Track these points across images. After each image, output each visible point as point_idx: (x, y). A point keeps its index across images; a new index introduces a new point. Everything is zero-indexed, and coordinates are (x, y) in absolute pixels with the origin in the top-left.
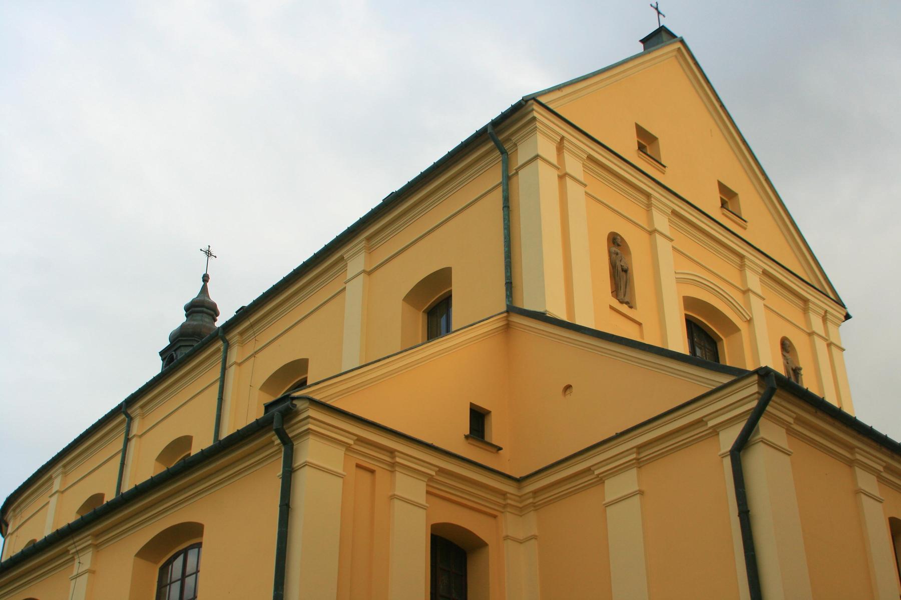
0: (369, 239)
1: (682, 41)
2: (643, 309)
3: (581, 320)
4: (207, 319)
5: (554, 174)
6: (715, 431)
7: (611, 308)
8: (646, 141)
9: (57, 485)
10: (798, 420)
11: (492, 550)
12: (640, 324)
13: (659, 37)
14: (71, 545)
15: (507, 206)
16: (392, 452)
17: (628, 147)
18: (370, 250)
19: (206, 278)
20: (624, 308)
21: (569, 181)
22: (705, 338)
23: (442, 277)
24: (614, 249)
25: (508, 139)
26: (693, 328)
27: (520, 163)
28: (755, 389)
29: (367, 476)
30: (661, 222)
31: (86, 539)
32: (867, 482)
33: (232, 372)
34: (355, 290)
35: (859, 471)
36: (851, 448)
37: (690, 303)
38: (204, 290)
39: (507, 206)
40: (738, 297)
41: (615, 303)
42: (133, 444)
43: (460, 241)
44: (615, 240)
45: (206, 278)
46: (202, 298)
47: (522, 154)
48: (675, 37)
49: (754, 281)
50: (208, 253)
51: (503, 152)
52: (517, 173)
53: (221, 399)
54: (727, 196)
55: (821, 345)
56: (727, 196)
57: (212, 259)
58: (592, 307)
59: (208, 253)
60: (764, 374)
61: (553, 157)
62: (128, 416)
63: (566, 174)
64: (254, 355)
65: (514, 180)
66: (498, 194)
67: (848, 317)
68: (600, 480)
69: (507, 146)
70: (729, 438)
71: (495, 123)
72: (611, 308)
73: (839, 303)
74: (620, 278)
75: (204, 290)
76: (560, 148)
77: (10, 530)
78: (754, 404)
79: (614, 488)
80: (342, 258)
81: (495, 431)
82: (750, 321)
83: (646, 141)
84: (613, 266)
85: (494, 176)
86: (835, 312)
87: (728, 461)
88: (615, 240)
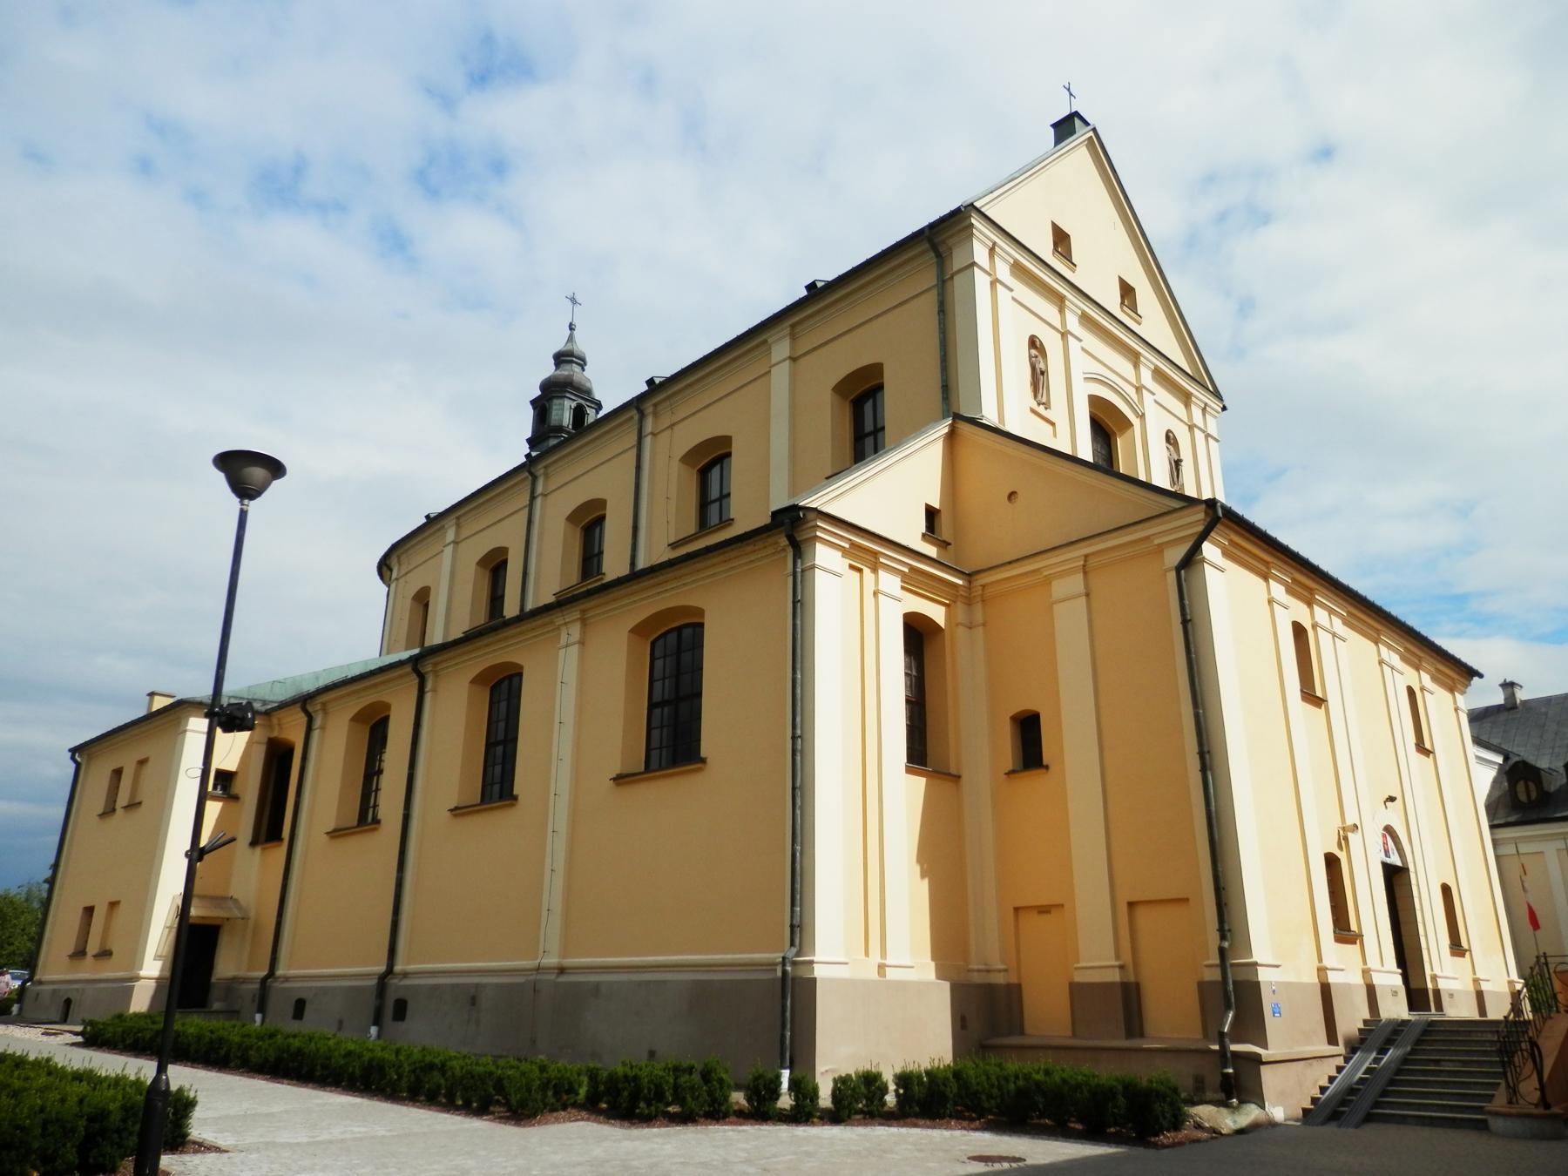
0: (793, 326)
1: (1094, 130)
2: (1058, 412)
3: (1010, 427)
4: (577, 369)
6: (1160, 548)
7: (1033, 411)
8: (1061, 239)
9: (450, 535)
12: (1053, 424)
13: (1065, 128)
16: (876, 554)
17: (1043, 245)
19: (571, 327)
20: (1041, 410)
21: (999, 286)
23: (875, 370)
24: (1034, 352)
27: (955, 268)
28: (1201, 516)
29: (857, 575)
30: (1073, 323)
31: (574, 614)
32: (1278, 590)
34: (780, 377)
37: (1095, 401)
38: (571, 339)
39: (943, 309)
40: (1132, 392)
42: (539, 501)
43: (890, 338)
44: (1034, 342)
45: (571, 327)
46: (569, 347)
47: (957, 262)
48: (1087, 124)
49: (1147, 377)
50: (573, 301)
51: (939, 255)
52: (952, 277)
53: (638, 468)
54: (1127, 291)
55: (1199, 435)
56: (1127, 291)
57: (577, 308)
59: (573, 301)
60: (1211, 504)
62: (531, 474)
63: (997, 280)
64: (671, 426)
65: (949, 284)
66: (932, 298)
67: (1224, 408)
69: (942, 249)
70: (1175, 555)
71: (932, 226)
72: (1033, 411)
73: (1217, 394)
74: (1038, 378)
75: (571, 339)
76: (992, 251)
77: (394, 575)
78: (1200, 528)
79: (1060, 588)
80: (765, 342)
82: (1142, 416)
83: (1061, 239)
84: (1033, 368)
85: (930, 278)
86: (1215, 404)
87: (1172, 576)
88: (1034, 342)
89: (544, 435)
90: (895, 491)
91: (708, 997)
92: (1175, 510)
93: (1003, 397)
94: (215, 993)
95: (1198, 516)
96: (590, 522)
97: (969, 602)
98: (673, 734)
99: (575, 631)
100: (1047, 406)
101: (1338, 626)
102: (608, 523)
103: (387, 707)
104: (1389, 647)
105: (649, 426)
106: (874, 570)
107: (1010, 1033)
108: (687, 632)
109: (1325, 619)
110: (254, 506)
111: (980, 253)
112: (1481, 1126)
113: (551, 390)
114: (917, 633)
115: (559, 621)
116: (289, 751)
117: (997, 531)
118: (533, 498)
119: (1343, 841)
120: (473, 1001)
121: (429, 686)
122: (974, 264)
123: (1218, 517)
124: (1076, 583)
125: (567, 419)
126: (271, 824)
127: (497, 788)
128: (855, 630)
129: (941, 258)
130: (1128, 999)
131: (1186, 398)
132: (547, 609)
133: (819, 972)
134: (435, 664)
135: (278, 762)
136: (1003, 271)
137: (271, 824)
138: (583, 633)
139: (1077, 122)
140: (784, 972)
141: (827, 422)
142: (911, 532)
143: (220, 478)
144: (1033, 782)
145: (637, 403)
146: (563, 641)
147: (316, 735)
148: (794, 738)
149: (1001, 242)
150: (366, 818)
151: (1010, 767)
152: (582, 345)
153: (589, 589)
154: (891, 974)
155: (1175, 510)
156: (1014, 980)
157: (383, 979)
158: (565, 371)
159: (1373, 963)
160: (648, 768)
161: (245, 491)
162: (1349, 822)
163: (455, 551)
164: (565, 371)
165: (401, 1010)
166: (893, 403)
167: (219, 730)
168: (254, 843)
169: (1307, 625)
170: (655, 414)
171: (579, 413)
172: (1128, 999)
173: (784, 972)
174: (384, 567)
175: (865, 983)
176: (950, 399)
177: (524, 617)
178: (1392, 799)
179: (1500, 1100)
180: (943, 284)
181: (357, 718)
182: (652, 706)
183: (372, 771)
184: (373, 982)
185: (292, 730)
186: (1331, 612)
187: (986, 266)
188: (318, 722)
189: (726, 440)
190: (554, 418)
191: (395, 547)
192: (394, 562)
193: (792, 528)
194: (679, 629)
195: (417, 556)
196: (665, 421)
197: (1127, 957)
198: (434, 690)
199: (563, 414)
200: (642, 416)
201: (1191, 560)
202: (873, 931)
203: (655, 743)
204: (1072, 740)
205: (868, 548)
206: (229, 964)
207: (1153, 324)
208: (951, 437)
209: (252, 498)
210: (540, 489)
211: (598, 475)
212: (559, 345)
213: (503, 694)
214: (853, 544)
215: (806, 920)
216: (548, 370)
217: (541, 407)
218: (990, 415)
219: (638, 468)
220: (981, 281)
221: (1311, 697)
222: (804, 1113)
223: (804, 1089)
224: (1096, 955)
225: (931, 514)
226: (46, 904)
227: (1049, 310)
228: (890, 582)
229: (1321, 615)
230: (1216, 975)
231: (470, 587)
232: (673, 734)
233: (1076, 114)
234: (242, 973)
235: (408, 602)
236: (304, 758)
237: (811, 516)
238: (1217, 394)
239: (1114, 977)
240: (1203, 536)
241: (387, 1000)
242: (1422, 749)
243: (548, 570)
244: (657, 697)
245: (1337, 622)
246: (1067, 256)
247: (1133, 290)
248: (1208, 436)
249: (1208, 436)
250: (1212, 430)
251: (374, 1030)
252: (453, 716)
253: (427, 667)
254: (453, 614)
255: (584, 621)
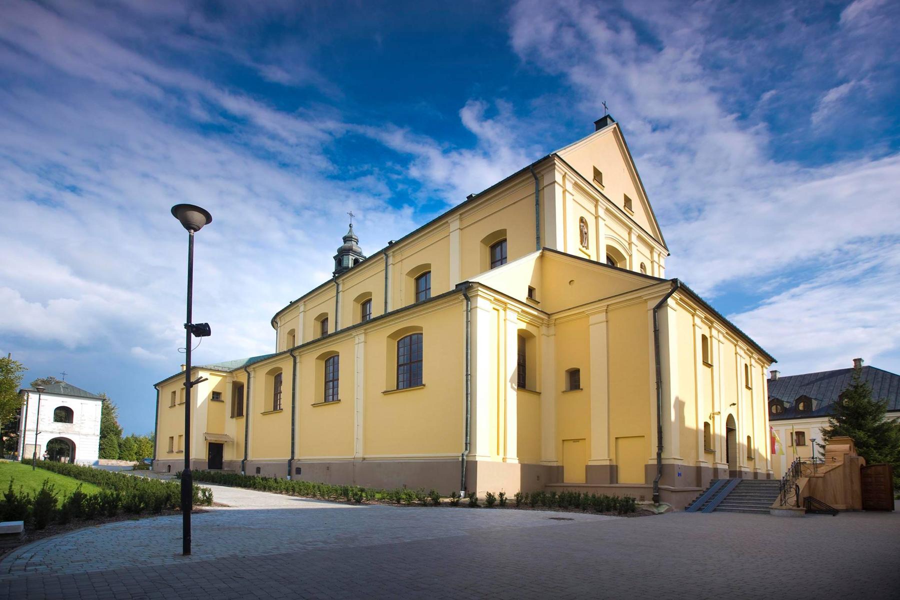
0: (461, 215)
4: (354, 243)
5: (561, 190)
6: (646, 301)
8: (598, 175)
9: (302, 308)
10: (681, 299)
11: (537, 338)
14: (354, 333)
15: (537, 203)
16: (505, 304)
18: (461, 219)
20: (584, 249)
22: (613, 261)
25: (539, 173)
26: (608, 258)
30: (601, 212)
31: (361, 330)
32: (698, 321)
33: (390, 268)
34: (455, 237)
35: (696, 317)
36: (695, 310)
37: (610, 248)
38: (350, 231)
41: (581, 247)
44: (582, 220)
47: (546, 181)
48: (613, 121)
51: (536, 179)
53: (386, 278)
54: (628, 201)
55: (656, 266)
56: (628, 201)
58: (574, 248)
61: (561, 183)
65: (541, 192)
66: (533, 197)
68: (588, 316)
74: (584, 236)
75: (350, 231)
76: (564, 177)
79: (592, 319)
81: (537, 296)
82: (631, 256)
83: (598, 175)
84: (581, 231)
85: (532, 189)
86: (665, 253)
88: (582, 220)
89: (341, 270)
90: (516, 275)
91: (429, 468)
92: (653, 285)
93: (566, 239)
94: (224, 465)
95: (668, 288)
96: (365, 302)
97: (548, 326)
98: (409, 371)
99: (362, 338)
100: (587, 248)
101: (721, 338)
102: (373, 302)
103: (281, 369)
104: (741, 348)
105: (390, 260)
106: (505, 310)
107: (558, 482)
108: (414, 337)
109: (718, 334)
110: (196, 235)
111: (558, 177)
112: (768, 513)
113: (342, 253)
114: (524, 339)
115: (354, 334)
116: (243, 386)
117: (560, 296)
118: (338, 293)
119: (712, 417)
120: (328, 468)
121: (298, 360)
122: (555, 182)
123: (677, 286)
124: (602, 317)
125: (351, 264)
126: (239, 410)
127: (331, 397)
128: (496, 335)
129: (537, 181)
130: (613, 471)
131: (652, 249)
132: (349, 329)
133: (478, 459)
134: (278, 548)
135: (238, 390)
136: (569, 186)
137: (239, 410)
138: (365, 338)
139: (609, 120)
140: (463, 459)
141: (481, 253)
142: (523, 296)
143: (177, 223)
144: (575, 395)
145: (385, 251)
146: (357, 342)
147: (252, 380)
148: (467, 375)
149: (570, 173)
150: (276, 407)
151: (564, 389)
152: (356, 234)
153: (366, 321)
154: (508, 461)
155: (653, 285)
156: (560, 464)
157: (290, 461)
158: (348, 244)
159: (718, 461)
160: (398, 388)
161: (190, 226)
162: (716, 411)
163: (304, 316)
164: (348, 244)
165: (298, 471)
166: (510, 247)
167: (193, 336)
168: (232, 417)
169: (708, 336)
170: (394, 256)
171: (356, 261)
172: (613, 471)
173: (463, 459)
174: (274, 322)
175: (498, 463)
176: (541, 241)
177: (337, 333)
178: (734, 404)
179: (776, 504)
180: (538, 192)
181: (269, 373)
182: (399, 366)
183: (277, 393)
184: (287, 462)
185: (242, 378)
186: (719, 331)
187: (561, 183)
188: (252, 376)
189: (429, 266)
190: (345, 264)
191: (278, 314)
192: (278, 320)
193: (466, 290)
194: (411, 336)
195: (287, 317)
196: (398, 258)
197: (613, 457)
198: (300, 362)
199: (349, 261)
200: (387, 257)
201: (662, 304)
202: (501, 446)
203: (401, 379)
204: (595, 379)
205: (502, 298)
206: (228, 455)
207: (639, 214)
208: (542, 257)
209: (195, 230)
210: (340, 289)
211: (366, 282)
212: (346, 234)
213: (331, 362)
214: (495, 299)
215: (473, 441)
216: (341, 244)
217: (339, 260)
218: (560, 248)
219: (386, 278)
220: (558, 190)
221: (707, 364)
222: (474, 504)
223: (472, 495)
224: (599, 455)
225: (531, 290)
226: (155, 439)
227: (590, 206)
228: (512, 316)
229: (714, 332)
230: (655, 462)
231: (312, 329)
232: (409, 371)
233: (608, 116)
234: (235, 459)
235: (286, 336)
236: (248, 388)
237: (475, 285)
238: (666, 248)
239: (608, 463)
240: (669, 295)
241: (293, 467)
242: (747, 387)
243: (349, 316)
244: (401, 362)
245: (721, 336)
246: (600, 182)
247: (630, 200)
248: (660, 266)
249: (660, 266)
250: (662, 263)
251: (289, 477)
252: (310, 370)
253: (296, 353)
254: (307, 331)
255: (366, 334)
